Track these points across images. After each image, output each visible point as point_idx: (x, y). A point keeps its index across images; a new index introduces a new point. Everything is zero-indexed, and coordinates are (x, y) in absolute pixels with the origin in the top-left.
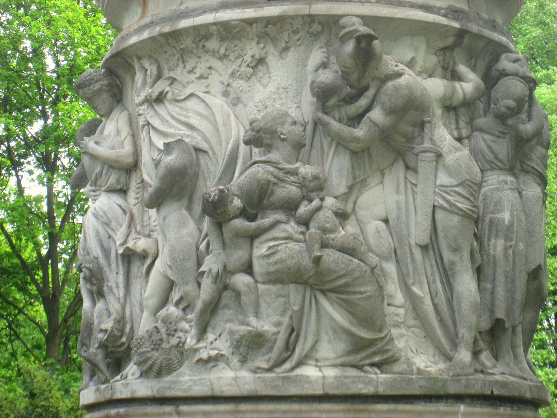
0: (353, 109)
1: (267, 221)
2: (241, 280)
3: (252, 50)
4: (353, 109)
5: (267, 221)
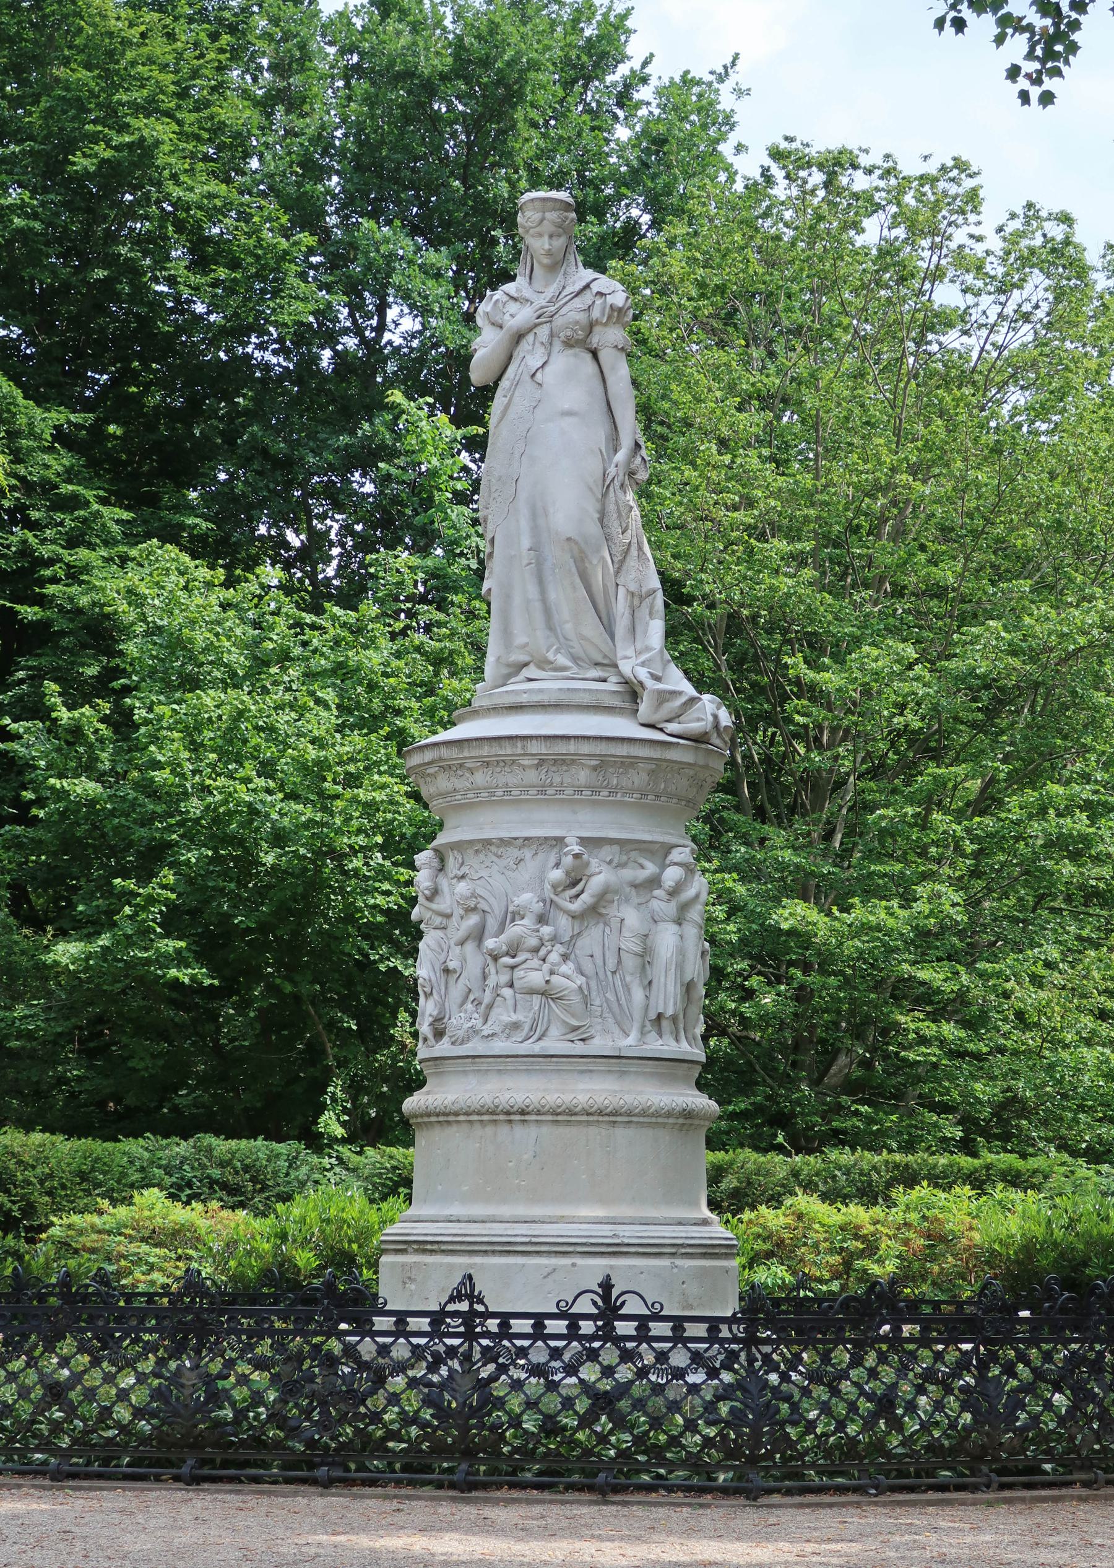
0: (574, 891)
1: (517, 960)
2: (507, 992)
3: (513, 853)
4: (574, 891)
5: (517, 960)
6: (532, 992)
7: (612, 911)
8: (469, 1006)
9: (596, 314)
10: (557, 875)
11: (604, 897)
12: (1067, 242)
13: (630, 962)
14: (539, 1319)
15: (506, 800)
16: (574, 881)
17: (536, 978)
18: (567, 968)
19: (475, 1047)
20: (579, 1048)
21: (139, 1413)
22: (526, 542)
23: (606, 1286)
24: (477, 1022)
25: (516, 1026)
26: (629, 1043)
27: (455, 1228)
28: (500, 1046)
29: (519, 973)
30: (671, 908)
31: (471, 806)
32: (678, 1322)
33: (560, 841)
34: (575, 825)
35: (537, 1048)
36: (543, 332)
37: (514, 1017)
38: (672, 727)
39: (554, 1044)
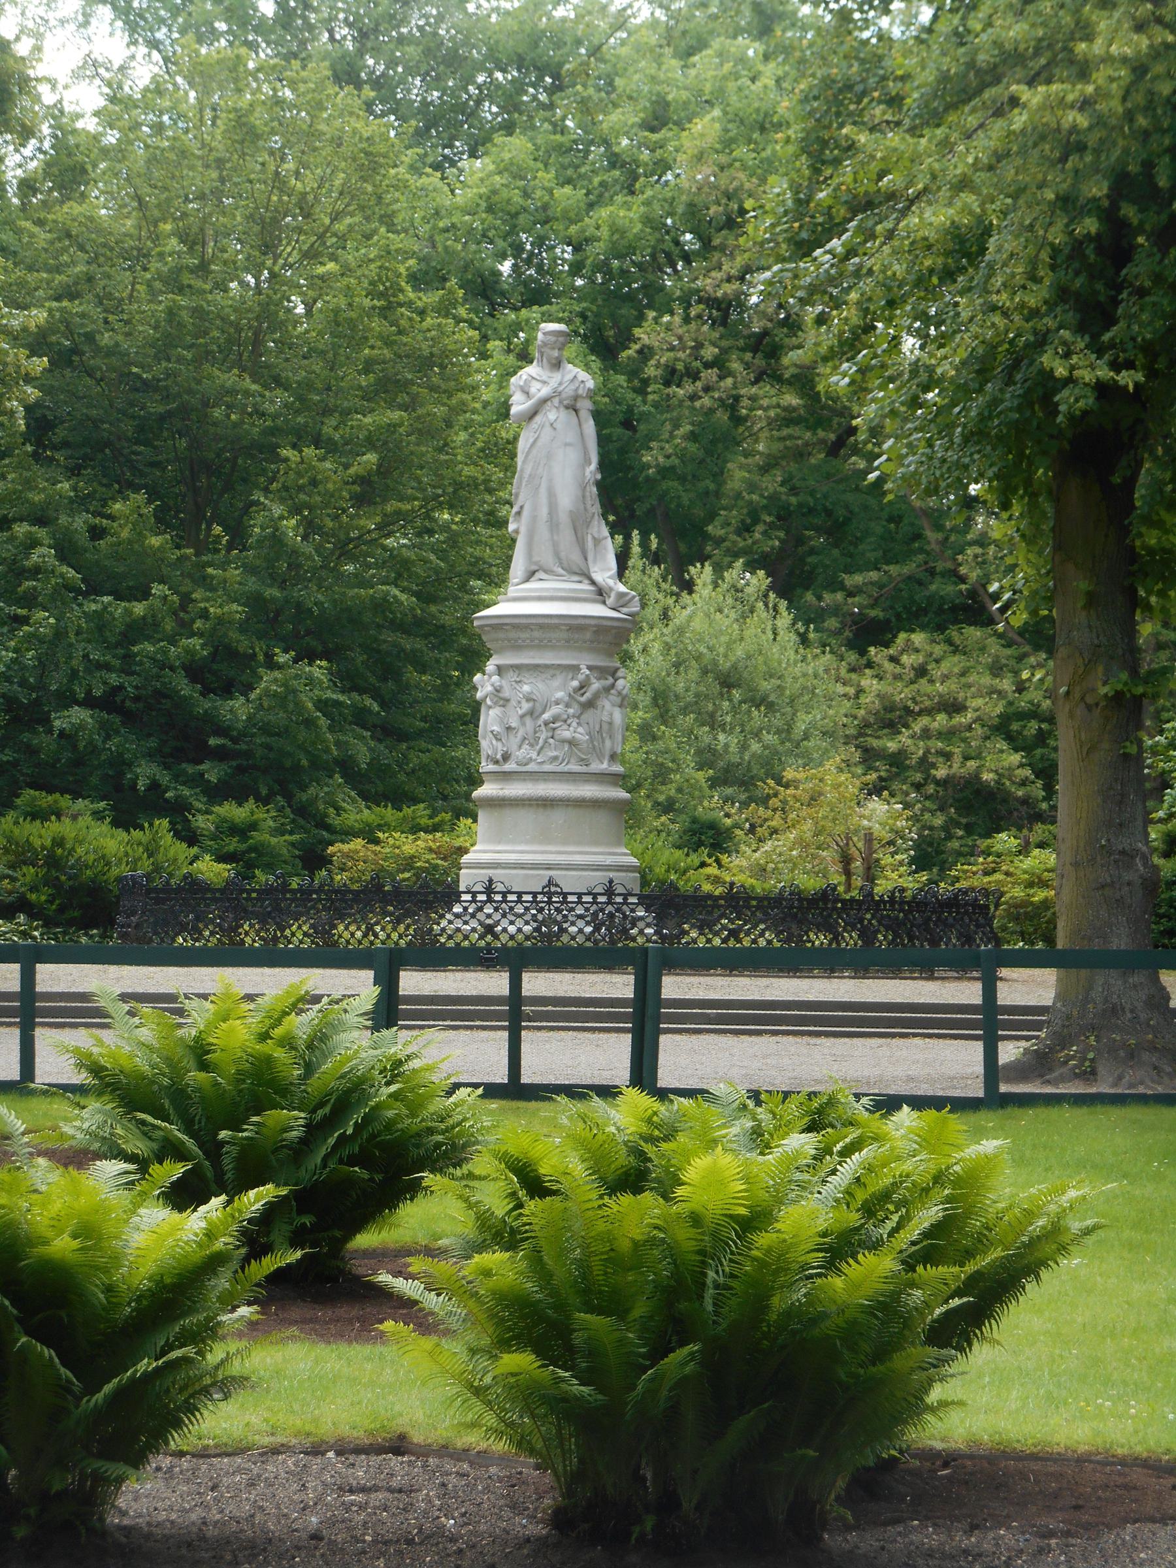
3: (552, 672)
6: (563, 741)
7: (599, 703)
8: (525, 746)
9: (580, 392)
10: (575, 683)
11: (596, 696)
12: (1116, 780)
13: (605, 727)
14: (580, 895)
15: (541, 646)
16: (583, 687)
17: (567, 734)
18: (580, 730)
19: (532, 767)
20: (584, 769)
21: (359, 929)
22: (544, 512)
23: (611, 881)
24: (534, 755)
25: (555, 758)
26: (604, 766)
27: (499, 848)
28: (548, 767)
29: (558, 732)
30: (618, 700)
31: (527, 647)
32: (520, 894)
33: (575, 669)
34: (584, 661)
35: (566, 769)
36: (556, 401)
37: (555, 753)
38: (625, 610)
39: (574, 767)
